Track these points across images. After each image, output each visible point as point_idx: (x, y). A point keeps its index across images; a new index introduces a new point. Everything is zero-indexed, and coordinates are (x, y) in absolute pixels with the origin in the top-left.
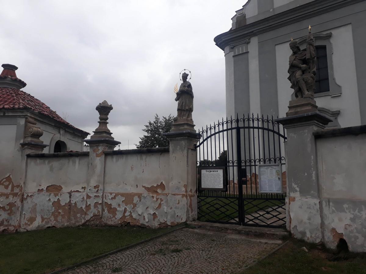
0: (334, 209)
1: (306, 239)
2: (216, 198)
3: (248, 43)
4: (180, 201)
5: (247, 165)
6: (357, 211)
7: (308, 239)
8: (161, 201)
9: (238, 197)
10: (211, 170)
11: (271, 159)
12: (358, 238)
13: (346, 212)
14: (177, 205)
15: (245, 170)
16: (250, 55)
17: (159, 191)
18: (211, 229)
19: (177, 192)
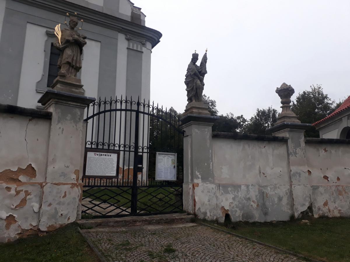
0: (223, 192)
1: (207, 218)
4: (67, 193)
6: (236, 192)
7: (208, 218)
8: (26, 195)
9: (132, 185)
10: (102, 154)
12: (237, 212)
13: (230, 194)
14: (62, 200)
15: (142, 156)
17: (22, 178)
18: (115, 225)
19: (62, 180)
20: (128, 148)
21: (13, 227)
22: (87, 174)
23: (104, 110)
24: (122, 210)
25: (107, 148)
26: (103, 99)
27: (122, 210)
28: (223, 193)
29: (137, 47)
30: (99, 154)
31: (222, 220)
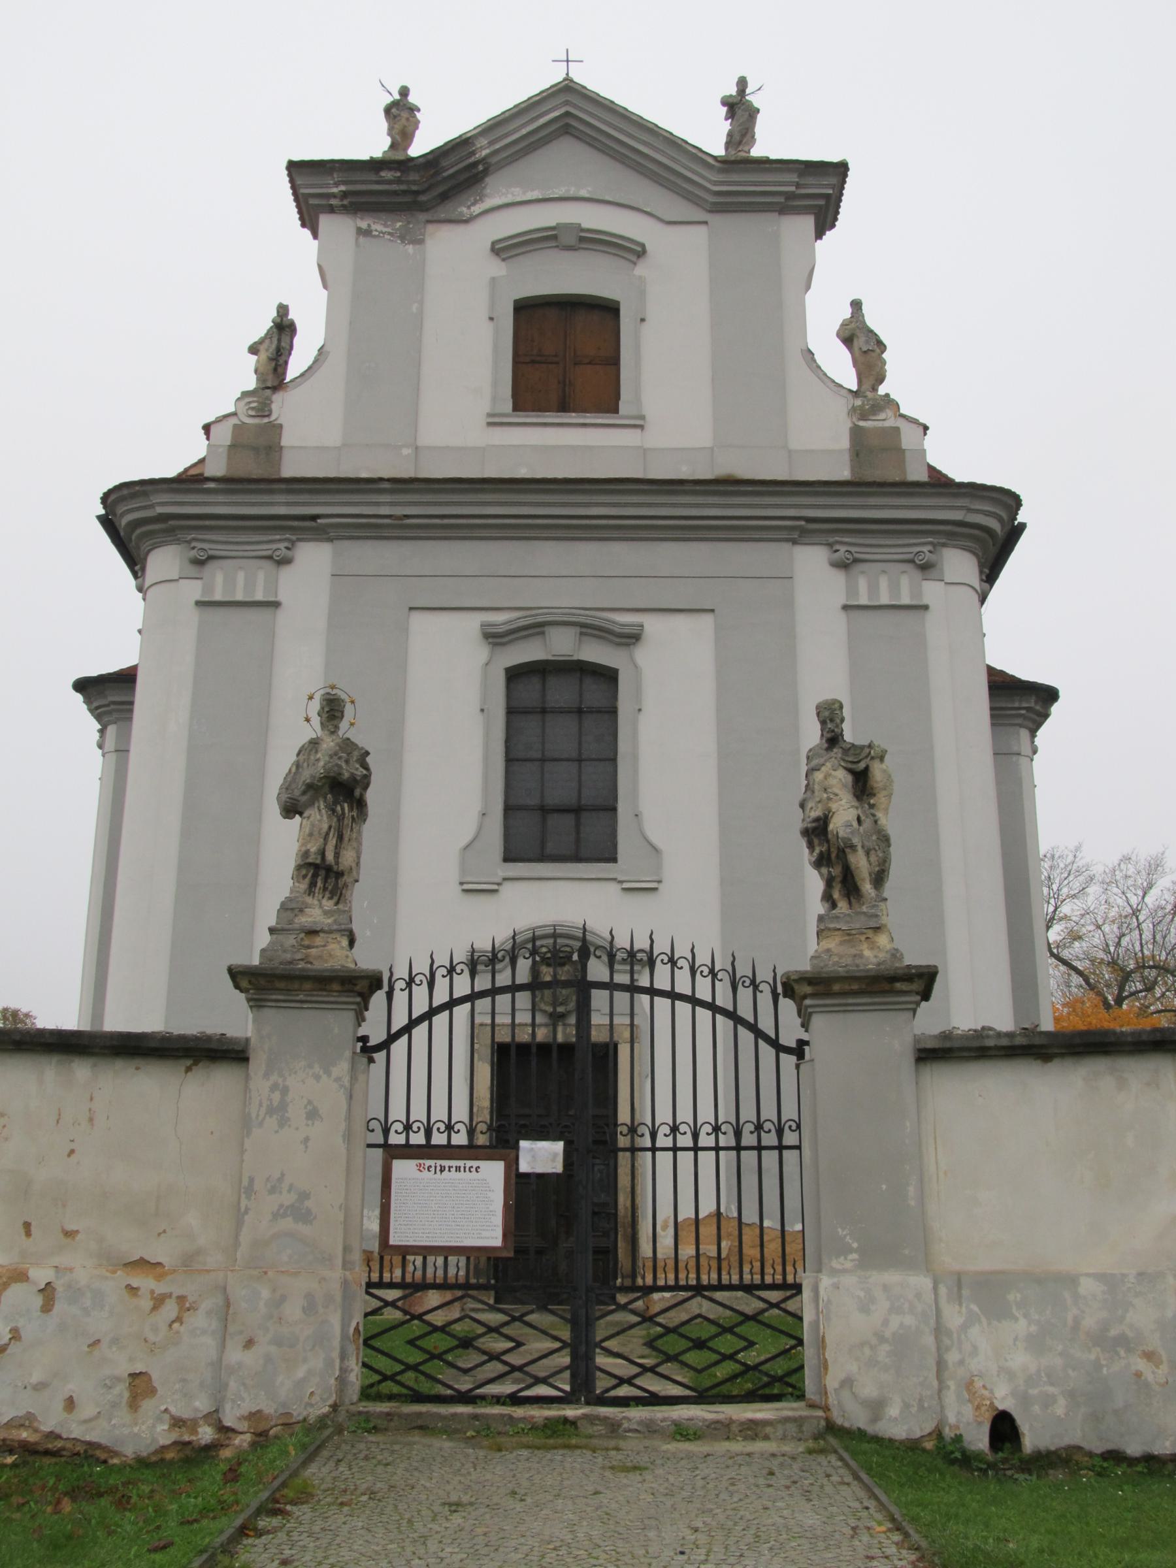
2: (459, 1293)
3: (285, 561)
5: (699, 1145)
10: (446, 1163)
11: (639, 1129)
16: (283, 617)
20: (689, 1135)
21: (149, 1406)
22: (393, 1241)
23: (448, 999)
24: (428, 1356)
25: (423, 1141)
26: (442, 960)
27: (428, 1356)
28: (979, 1313)
29: (895, 588)
30: (433, 1165)
31: (979, 1440)
